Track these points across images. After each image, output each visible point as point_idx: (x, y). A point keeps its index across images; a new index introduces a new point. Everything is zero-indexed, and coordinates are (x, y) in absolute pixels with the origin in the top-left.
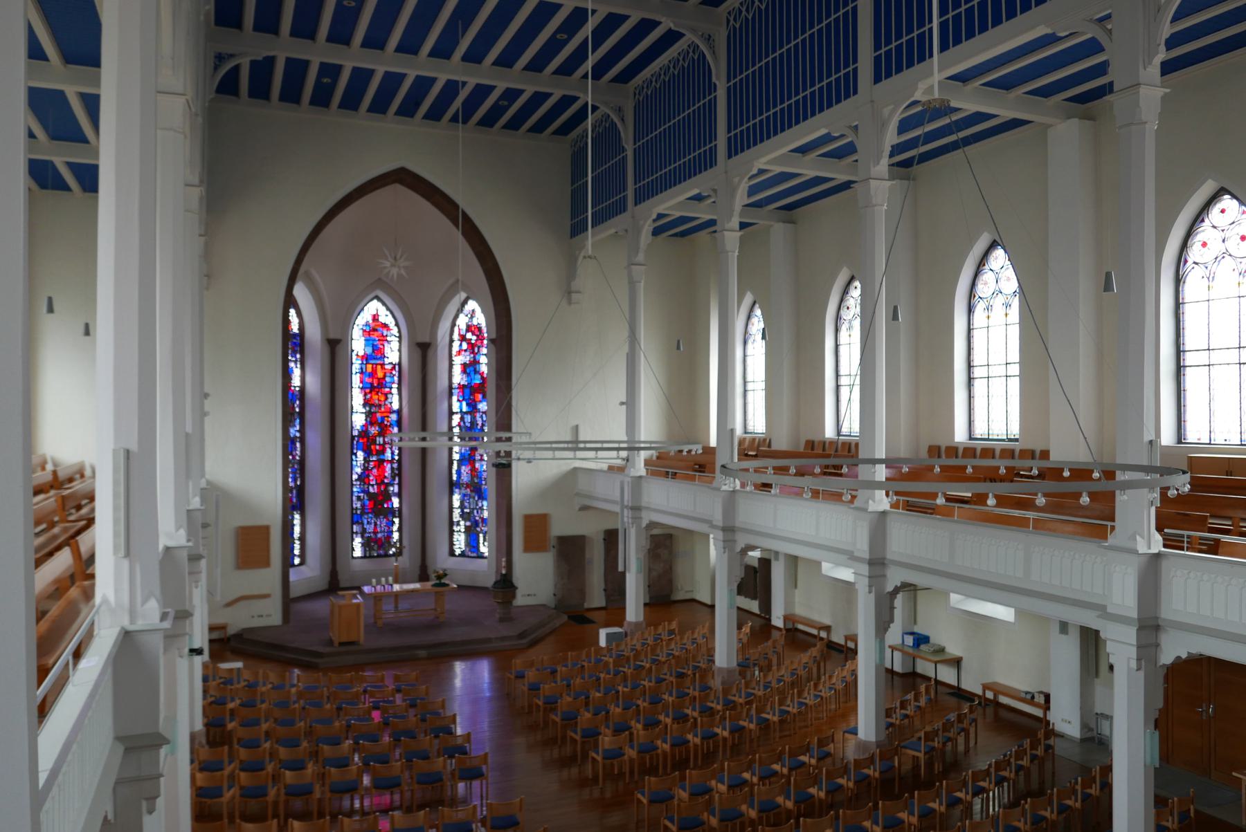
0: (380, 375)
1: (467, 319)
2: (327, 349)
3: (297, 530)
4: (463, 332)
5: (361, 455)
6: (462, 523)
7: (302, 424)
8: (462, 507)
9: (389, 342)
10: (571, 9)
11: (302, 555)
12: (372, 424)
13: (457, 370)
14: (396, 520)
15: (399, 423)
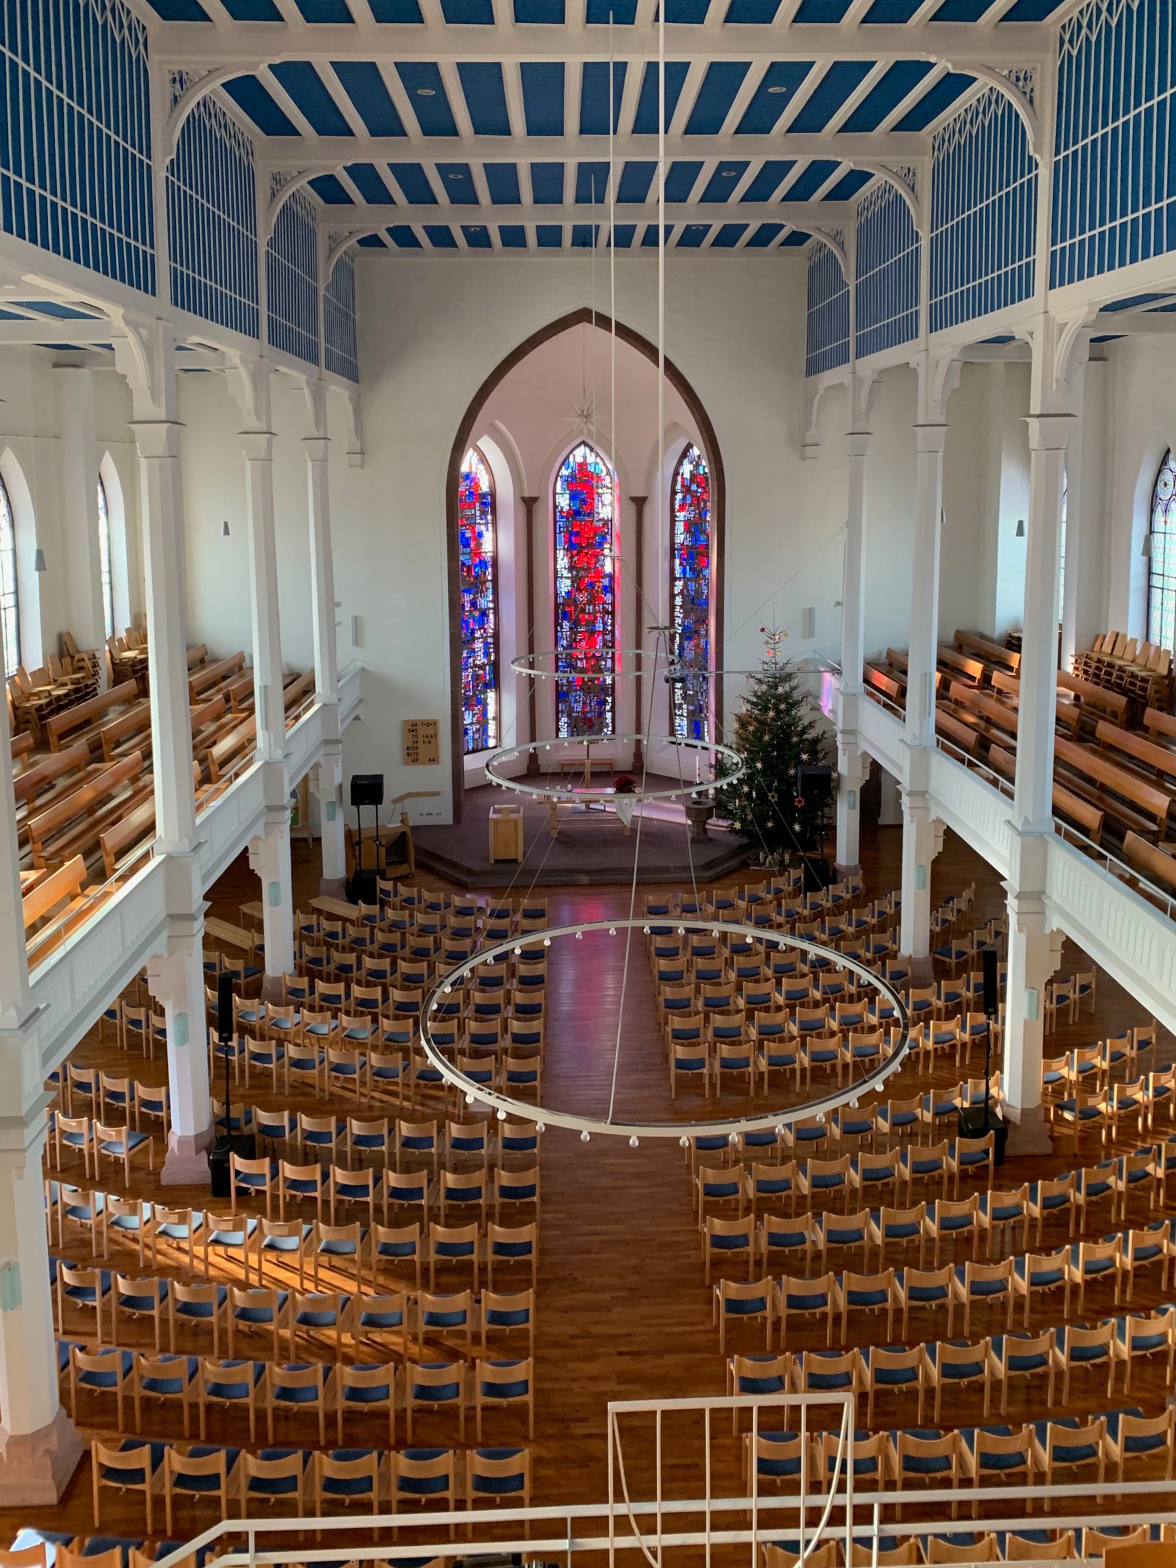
1: (691, 467)
2: (522, 508)
3: (491, 713)
4: (687, 483)
6: (685, 706)
9: (600, 495)
10: (645, 230)
11: (499, 737)
12: (579, 590)
13: (680, 527)
14: (609, 699)
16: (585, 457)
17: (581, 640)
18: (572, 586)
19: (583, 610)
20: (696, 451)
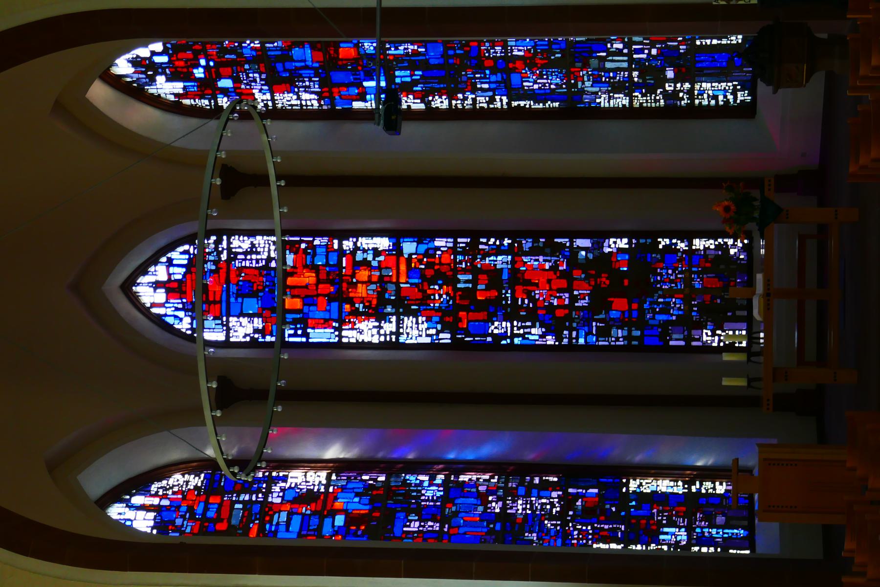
0: (309, 278)
3: (664, 485)
4: (193, 87)
5: (497, 327)
6: (669, 87)
7: (416, 467)
8: (627, 87)
12: (425, 299)
13: (286, 100)
14: (664, 242)
15: (422, 235)
16: (157, 285)
17: (532, 299)
18: (415, 314)
19: (469, 294)
20: (123, 67)
